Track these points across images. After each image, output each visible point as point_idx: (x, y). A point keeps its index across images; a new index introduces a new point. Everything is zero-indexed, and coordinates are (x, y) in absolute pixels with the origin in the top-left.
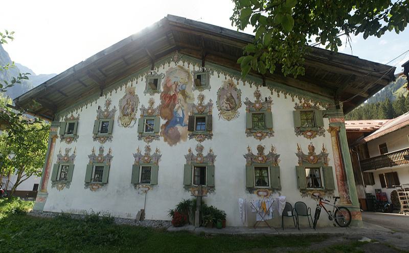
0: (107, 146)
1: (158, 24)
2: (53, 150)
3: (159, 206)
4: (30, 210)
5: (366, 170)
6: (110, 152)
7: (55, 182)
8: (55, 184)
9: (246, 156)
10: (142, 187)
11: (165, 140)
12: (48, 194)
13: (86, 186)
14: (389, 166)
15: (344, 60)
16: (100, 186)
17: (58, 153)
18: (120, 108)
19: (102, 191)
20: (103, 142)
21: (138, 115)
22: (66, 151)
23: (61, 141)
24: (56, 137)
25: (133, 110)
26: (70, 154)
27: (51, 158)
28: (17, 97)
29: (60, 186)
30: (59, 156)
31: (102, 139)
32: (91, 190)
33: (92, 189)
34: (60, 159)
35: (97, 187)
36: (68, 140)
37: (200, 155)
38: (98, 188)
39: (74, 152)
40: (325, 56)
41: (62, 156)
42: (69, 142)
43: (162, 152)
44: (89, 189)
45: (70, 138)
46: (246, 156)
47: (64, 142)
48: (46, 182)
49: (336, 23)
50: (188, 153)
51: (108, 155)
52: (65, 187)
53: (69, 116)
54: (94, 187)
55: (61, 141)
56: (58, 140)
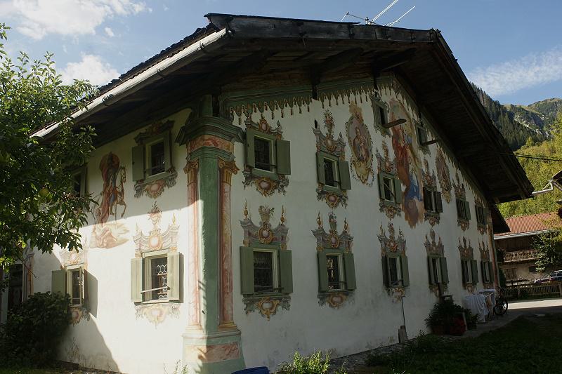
0: (340, 213)
1: (106, 353)
2: (228, 205)
3: (415, 316)
4: (516, 120)
5: (221, 39)
6: (346, 228)
7: (250, 301)
8: (252, 302)
9: (316, 233)
10: (154, 307)
11: (406, 218)
12: (240, 334)
13: (321, 299)
14: (189, 65)
15: (197, 308)
16: (344, 297)
17: (243, 218)
18: (350, 142)
19: (349, 307)
20: (334, 204)
21: (375, 164)
22: (262, 214)
23: (246, 183)
24: (232, 167)
25: (367, 152)
26: (274, 223)
27: (227, 228)
28: (316, 293)
29: (267, 306)
30: (247, 225)
31: (332, 198)
32: (330, 306)
33: (333, 305)
34: (250, 234)
35: (340, 299)
36: (264, 185)
37: (265, 225)
38: (342, 300)
39: (283, 220)
40: (329, 32)
41: (255, 227)
42: (267, 191)
43: (406, 237)
44: (327, 304)
45: (269, 179)
46: (316, 233)
47: (252, 188)
48: (227, 302)
49: (151, 10)
50: (317, 226)
51: (345, 233)
52: (280, 307)
53: (256, 117)
54: (335, 299)
55: (246, 183)
56: (237, 179)
